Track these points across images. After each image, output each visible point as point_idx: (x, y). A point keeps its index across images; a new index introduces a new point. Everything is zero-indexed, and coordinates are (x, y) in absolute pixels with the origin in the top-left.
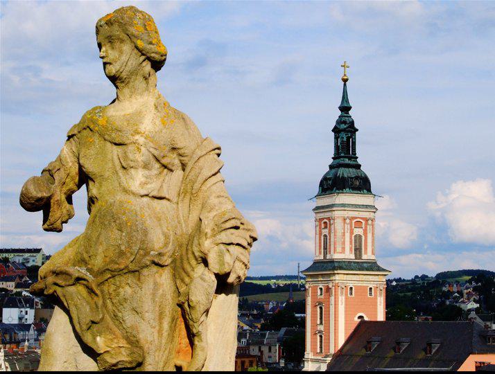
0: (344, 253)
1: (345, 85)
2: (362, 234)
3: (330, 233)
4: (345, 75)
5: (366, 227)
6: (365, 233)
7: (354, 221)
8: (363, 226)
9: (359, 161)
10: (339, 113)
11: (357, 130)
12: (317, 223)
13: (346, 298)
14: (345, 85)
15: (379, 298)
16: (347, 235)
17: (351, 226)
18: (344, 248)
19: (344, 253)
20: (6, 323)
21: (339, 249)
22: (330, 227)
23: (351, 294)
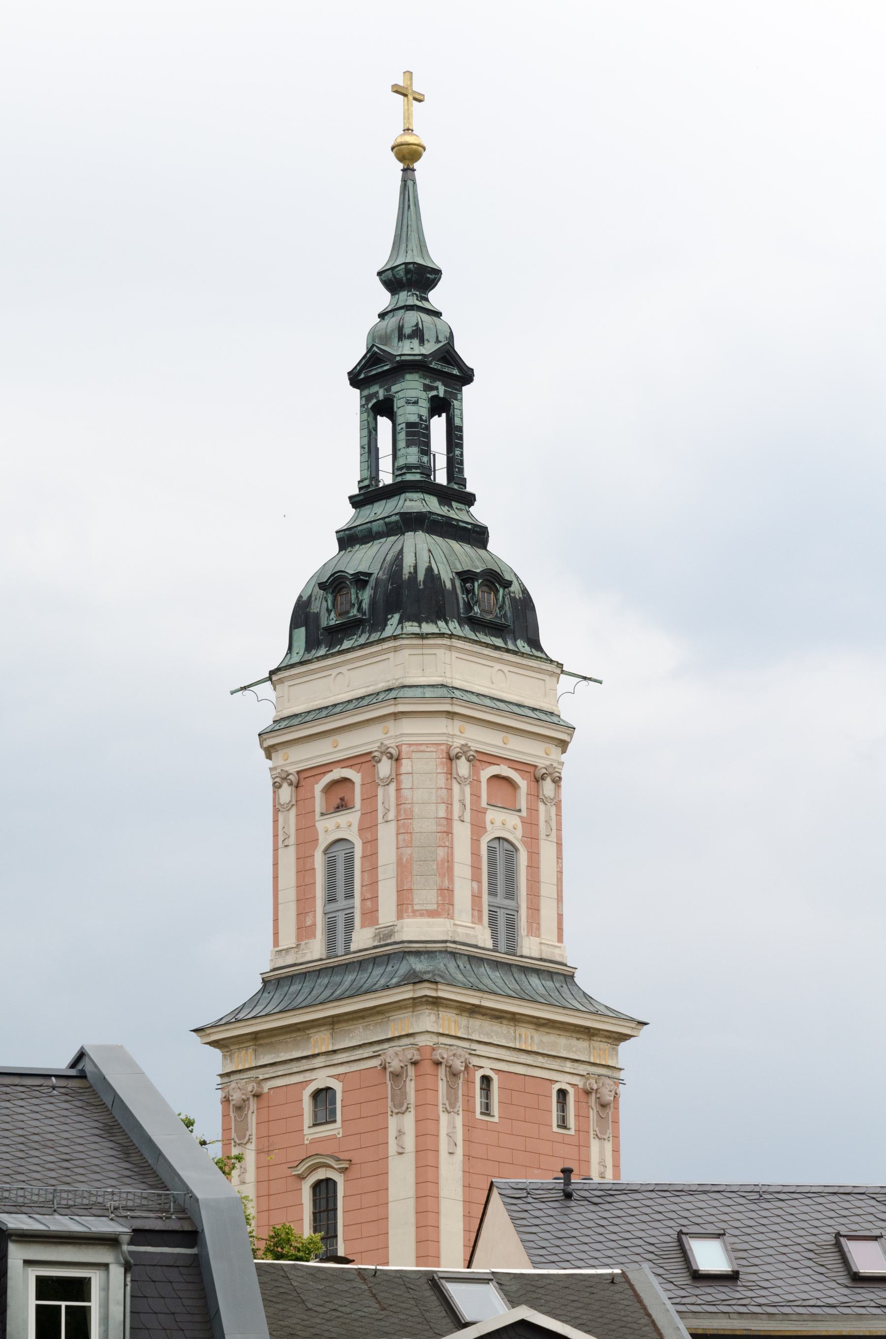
0: (450, 916)
1: (408, 171)
2: (516, 837)
3: (368, 828)
4: (408, 130)
5: (533, 811)
6: (368, 828)
7: (488, 772)
8: (523, 802)
9: (466, 475)
10: (384, 299)
11: (467, 376)
12: (286, 793)
13: (469, 1127)
14: (408, 171)
15: (595, 1145)
16: (462, 833)
17: (476, 796)
18: (447, 894)
19: (450, 916)
20: (410, 533)
21: (426, 897)
22: (370, 799)
23: (487, 1109)
